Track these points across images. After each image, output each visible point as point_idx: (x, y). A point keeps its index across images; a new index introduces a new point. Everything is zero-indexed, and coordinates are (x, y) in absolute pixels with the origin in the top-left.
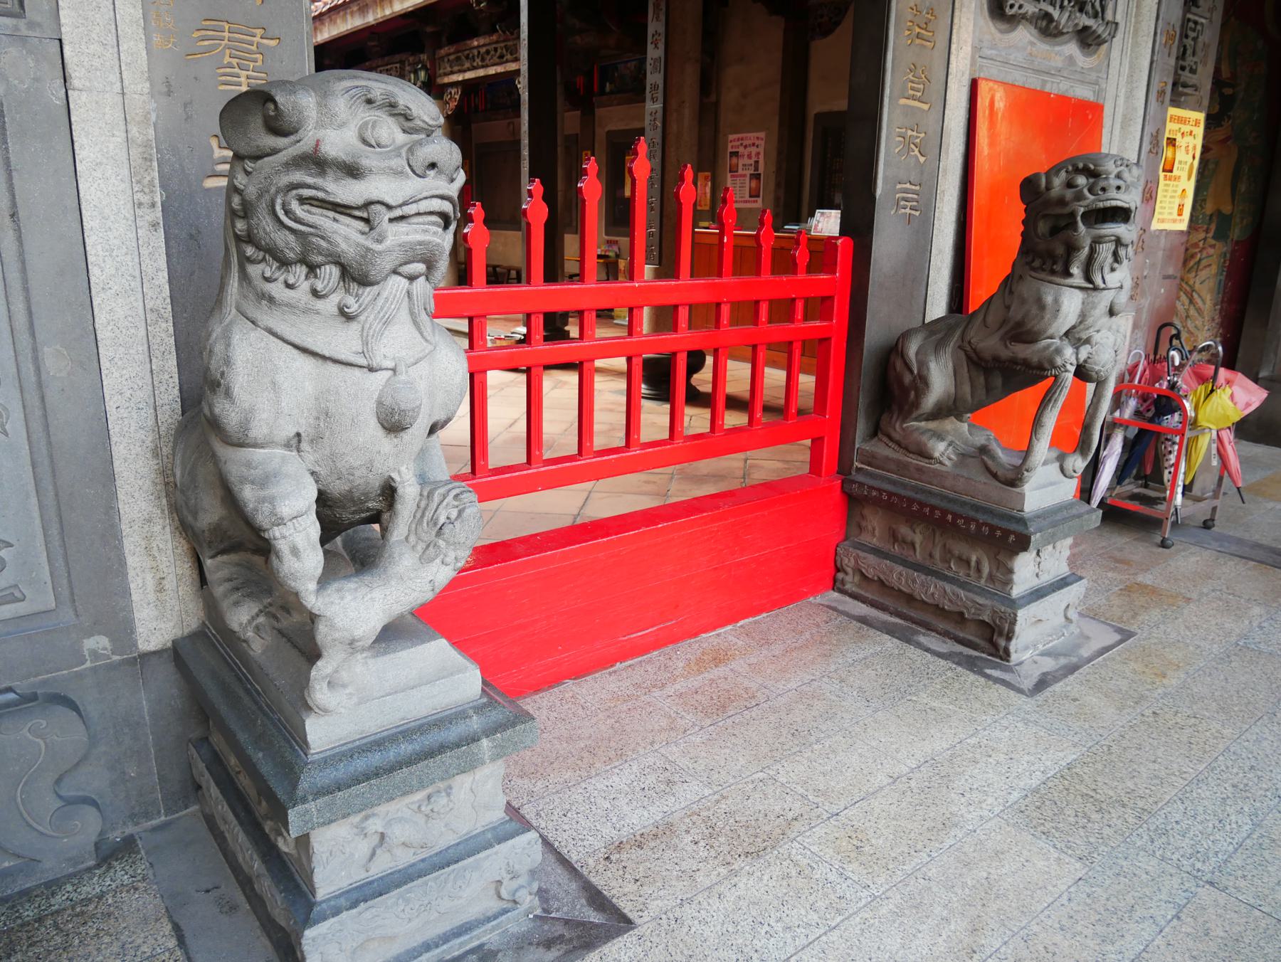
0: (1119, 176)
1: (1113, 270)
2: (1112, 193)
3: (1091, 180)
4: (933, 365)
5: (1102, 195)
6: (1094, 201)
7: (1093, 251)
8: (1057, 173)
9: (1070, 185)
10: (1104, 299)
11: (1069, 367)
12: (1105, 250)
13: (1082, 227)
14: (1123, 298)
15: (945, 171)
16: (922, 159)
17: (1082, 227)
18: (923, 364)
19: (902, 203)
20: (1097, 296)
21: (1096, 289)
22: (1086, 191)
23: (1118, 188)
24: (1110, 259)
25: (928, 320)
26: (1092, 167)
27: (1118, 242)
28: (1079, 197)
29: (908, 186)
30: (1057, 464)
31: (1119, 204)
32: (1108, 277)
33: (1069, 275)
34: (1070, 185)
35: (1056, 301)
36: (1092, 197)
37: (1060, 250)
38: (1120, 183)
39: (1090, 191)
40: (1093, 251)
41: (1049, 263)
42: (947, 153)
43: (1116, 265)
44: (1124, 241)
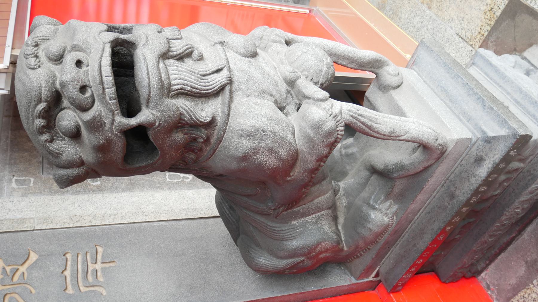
0: (58, 59)
1: (201, 58)
2: (90, 74)
3: (65, 103)
4: (295, 244)
5: (94, 90)
6: (105, 104)
7: (182, 93)
8: (57, 155)
9: (75, 135)
10: (240, 66)
11: (336, 111)
12: (181, 74)
13: (144, 116)
14: (237, 40)
15: (45, 220)
16: (34, 257)
17: (144, 116)
18: (293, 254)
19: (90, 278)
20: (239, 77)
21: (231, 82)
22: (88, 116)
23: (79, 63)
24: (188, 63)
25: (218, 215)
26: (41, 106)
27: (165, 56)
28: (95, 126)
29: (67, 273)
30: (392, 92)
31: (107, 60)
32: (209, 65)
33: (212, 123)
34: (75, 135)
35: (250, 135)
36: (97, 108)
37: (179, 137)
38: (70, 59)
39: (84, 109)
40: (182, 93)
41: (195, 145)
42: (23, 221)
43: (195, 54)
44: (164, 49)
